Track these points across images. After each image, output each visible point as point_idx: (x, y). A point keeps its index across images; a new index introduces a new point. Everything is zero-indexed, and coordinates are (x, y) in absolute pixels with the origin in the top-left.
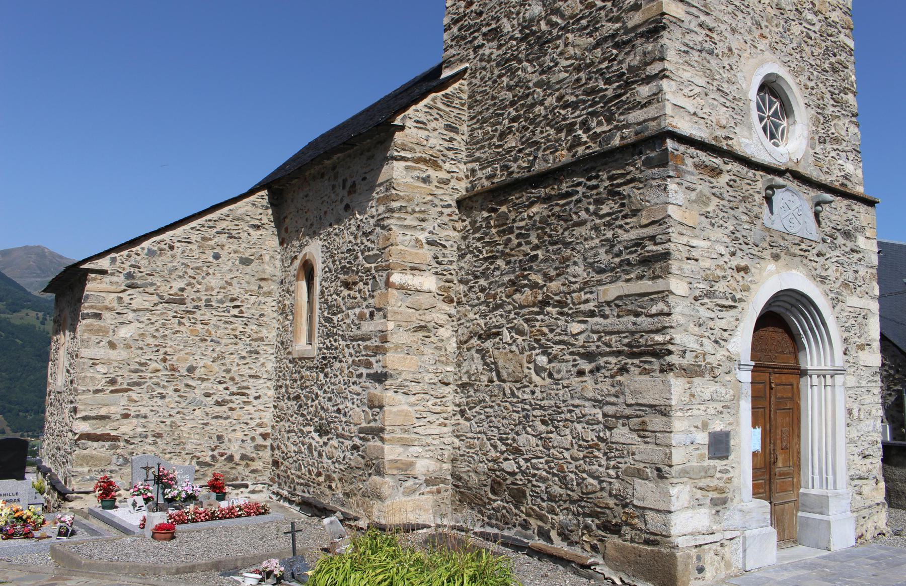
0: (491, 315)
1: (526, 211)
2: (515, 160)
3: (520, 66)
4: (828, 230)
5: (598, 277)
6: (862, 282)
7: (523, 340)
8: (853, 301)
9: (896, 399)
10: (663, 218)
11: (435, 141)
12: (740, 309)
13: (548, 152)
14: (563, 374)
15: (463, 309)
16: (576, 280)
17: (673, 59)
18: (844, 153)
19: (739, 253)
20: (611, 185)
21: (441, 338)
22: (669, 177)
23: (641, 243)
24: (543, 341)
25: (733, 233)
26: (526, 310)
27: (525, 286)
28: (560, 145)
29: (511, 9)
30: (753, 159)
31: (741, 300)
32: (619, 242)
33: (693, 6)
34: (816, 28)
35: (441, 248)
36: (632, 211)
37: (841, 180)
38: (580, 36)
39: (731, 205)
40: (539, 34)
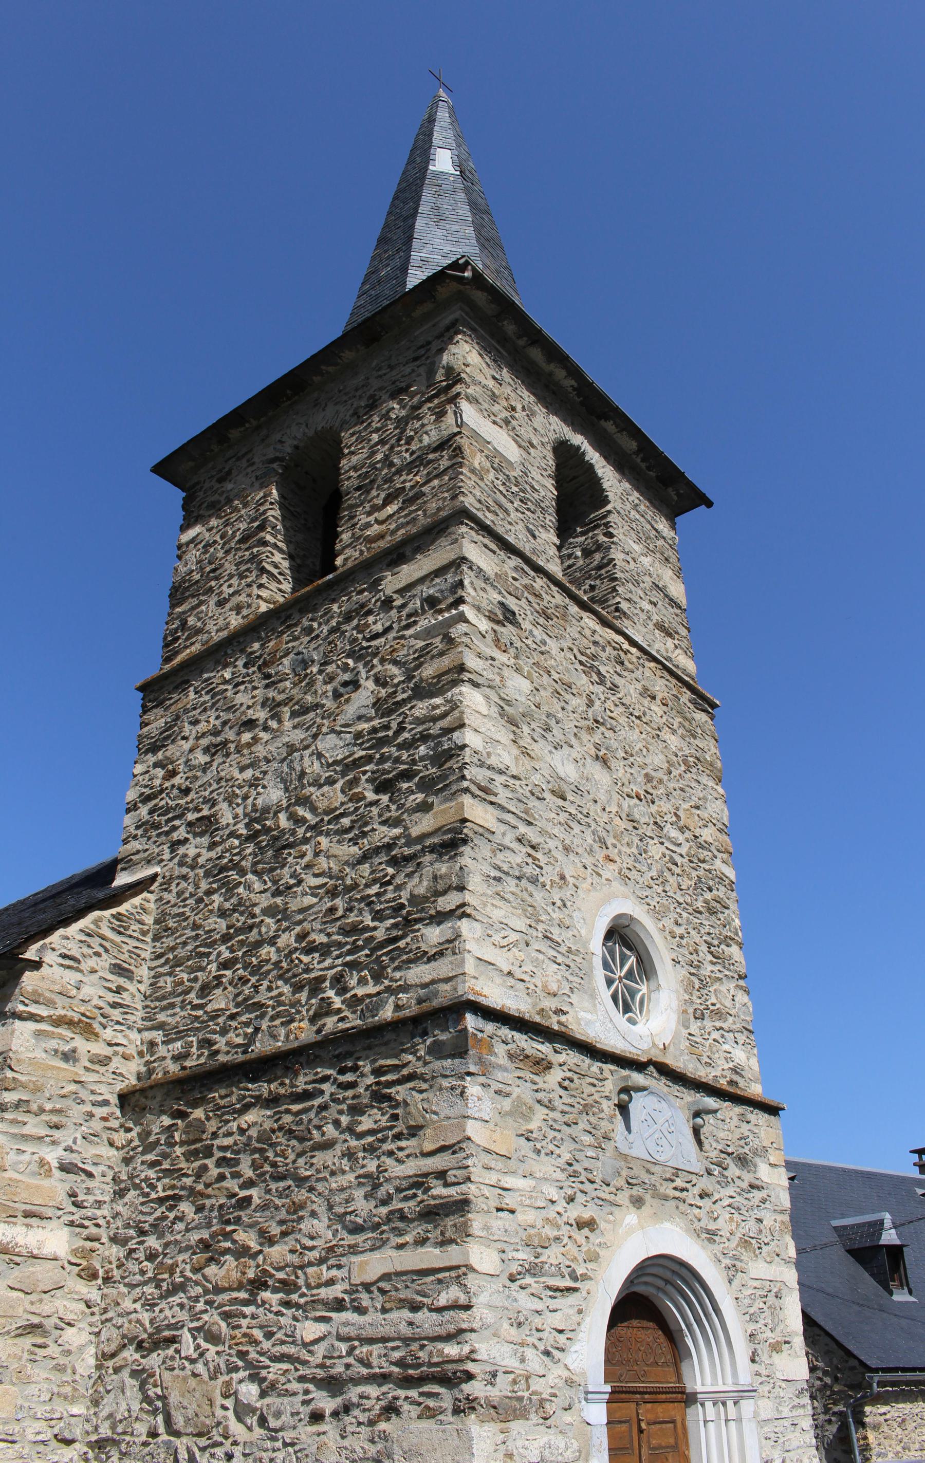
0: (163, 1304)
1: (235, 1119)
2: (224, 1032)
3: (243, 880)
4: (714, 1154)
5: (350, 1240)
6: (770, 1238)
7: (218, 1353)
8: (759, 1269)
9: (839, 1429)
10: (459, 1142)
11: (92, 991)
12: (584, 1293)
13: (277, 1022)
14: (286, 1418)
15: (114, 1291)
16: (314, 1243)
17: (478, 889)
18: (731, 1034)
19: (580, 1198)
20: (377, 1083)
21: (67, 1347)
22: (469, 1074)
23: (423, 1183)
24: (253, 1355)
25: (570, 1165)
26: (225, 1297)
27: (227, 1251)
28: (299, 1012)
29: (235, 789)
30: (598, 1045)
31: (585, 1277)
32: (387, 1180)
33: (509, 812)
34: (684, 850)
35: (84, 1177)
36: (409, 1128)
37: (729, 1075)
38: (339, 842)
39: (567, 1118)
40: (275, 833)
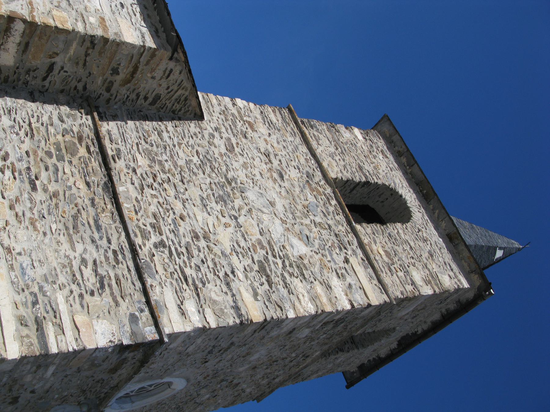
2: (128, 167)
